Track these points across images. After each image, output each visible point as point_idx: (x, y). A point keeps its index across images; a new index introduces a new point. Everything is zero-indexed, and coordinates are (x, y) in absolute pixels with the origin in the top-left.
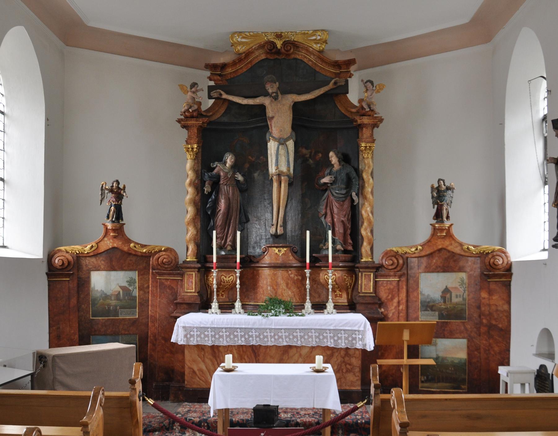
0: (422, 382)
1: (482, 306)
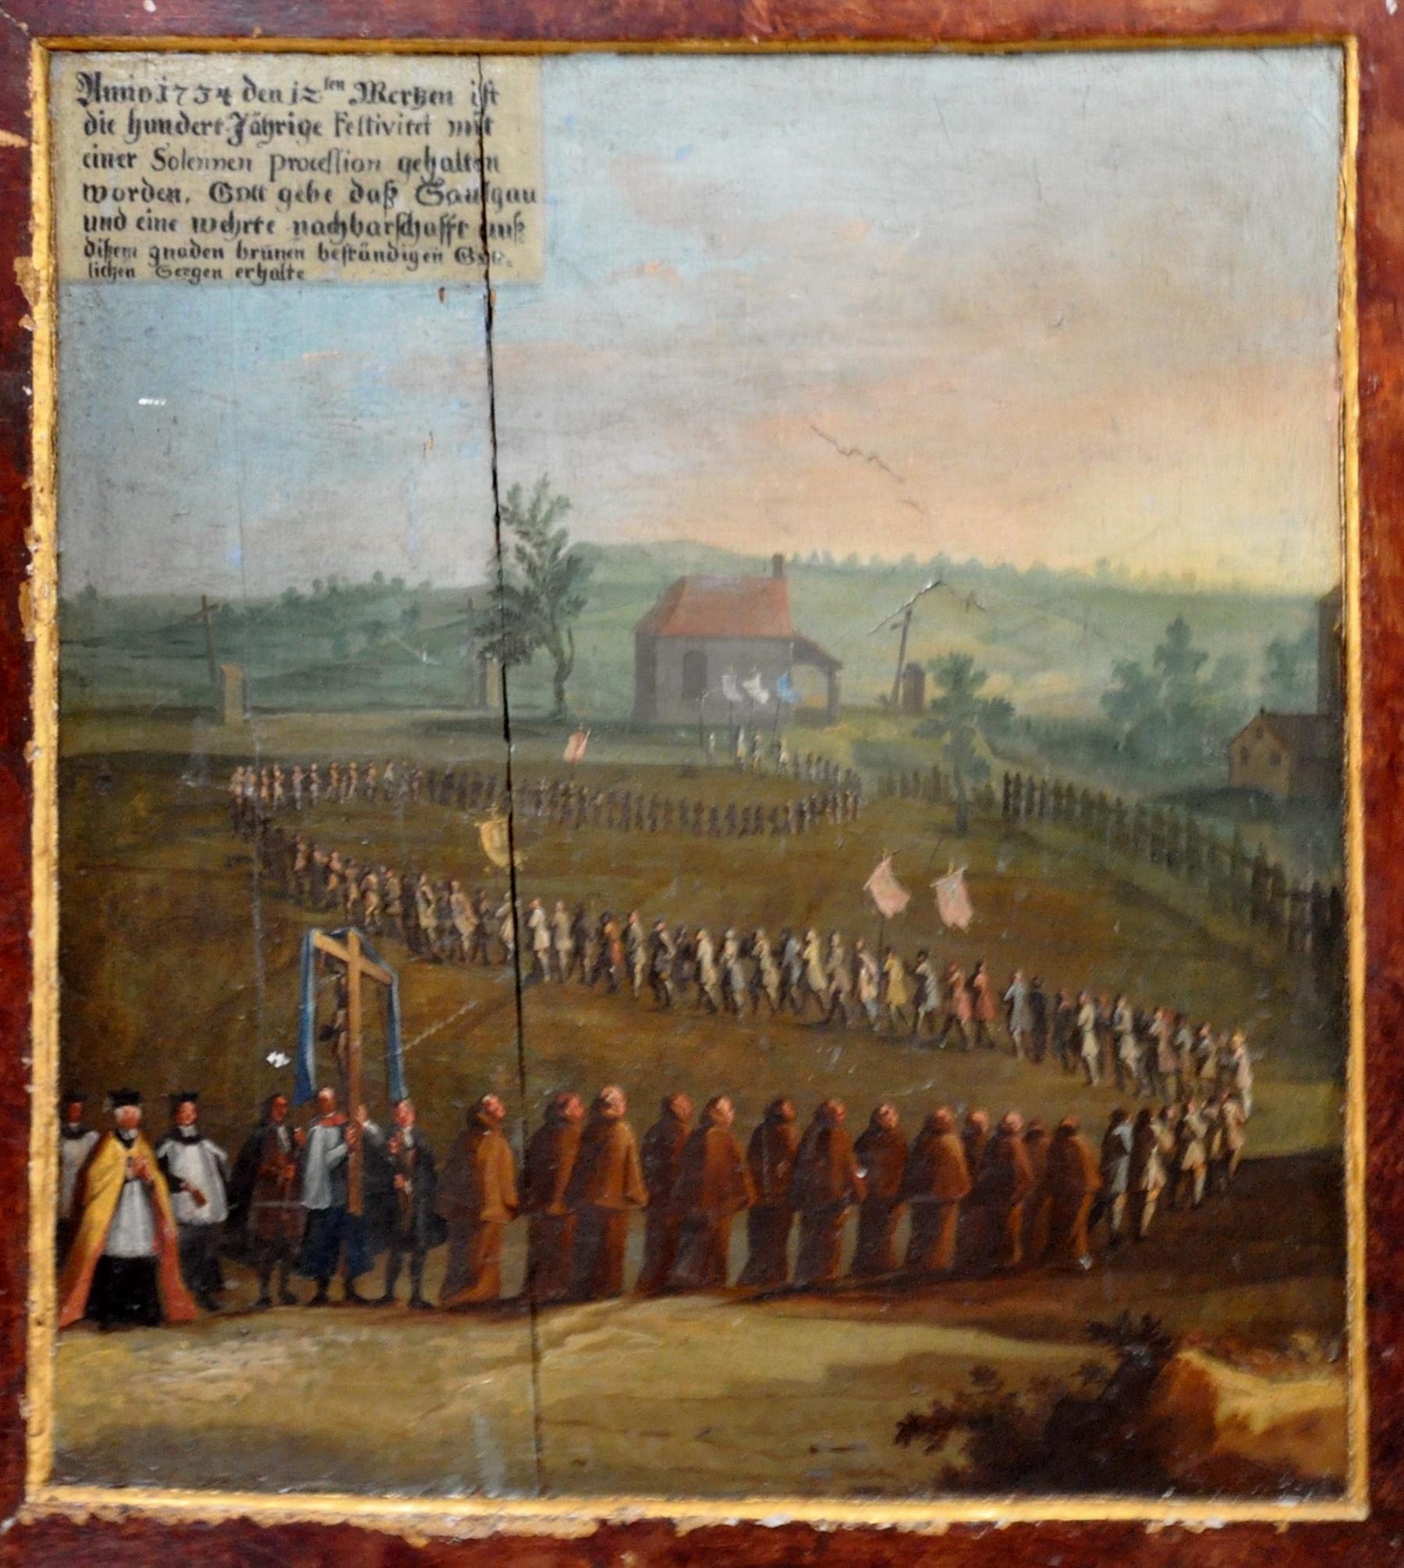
0: (119, 1297)
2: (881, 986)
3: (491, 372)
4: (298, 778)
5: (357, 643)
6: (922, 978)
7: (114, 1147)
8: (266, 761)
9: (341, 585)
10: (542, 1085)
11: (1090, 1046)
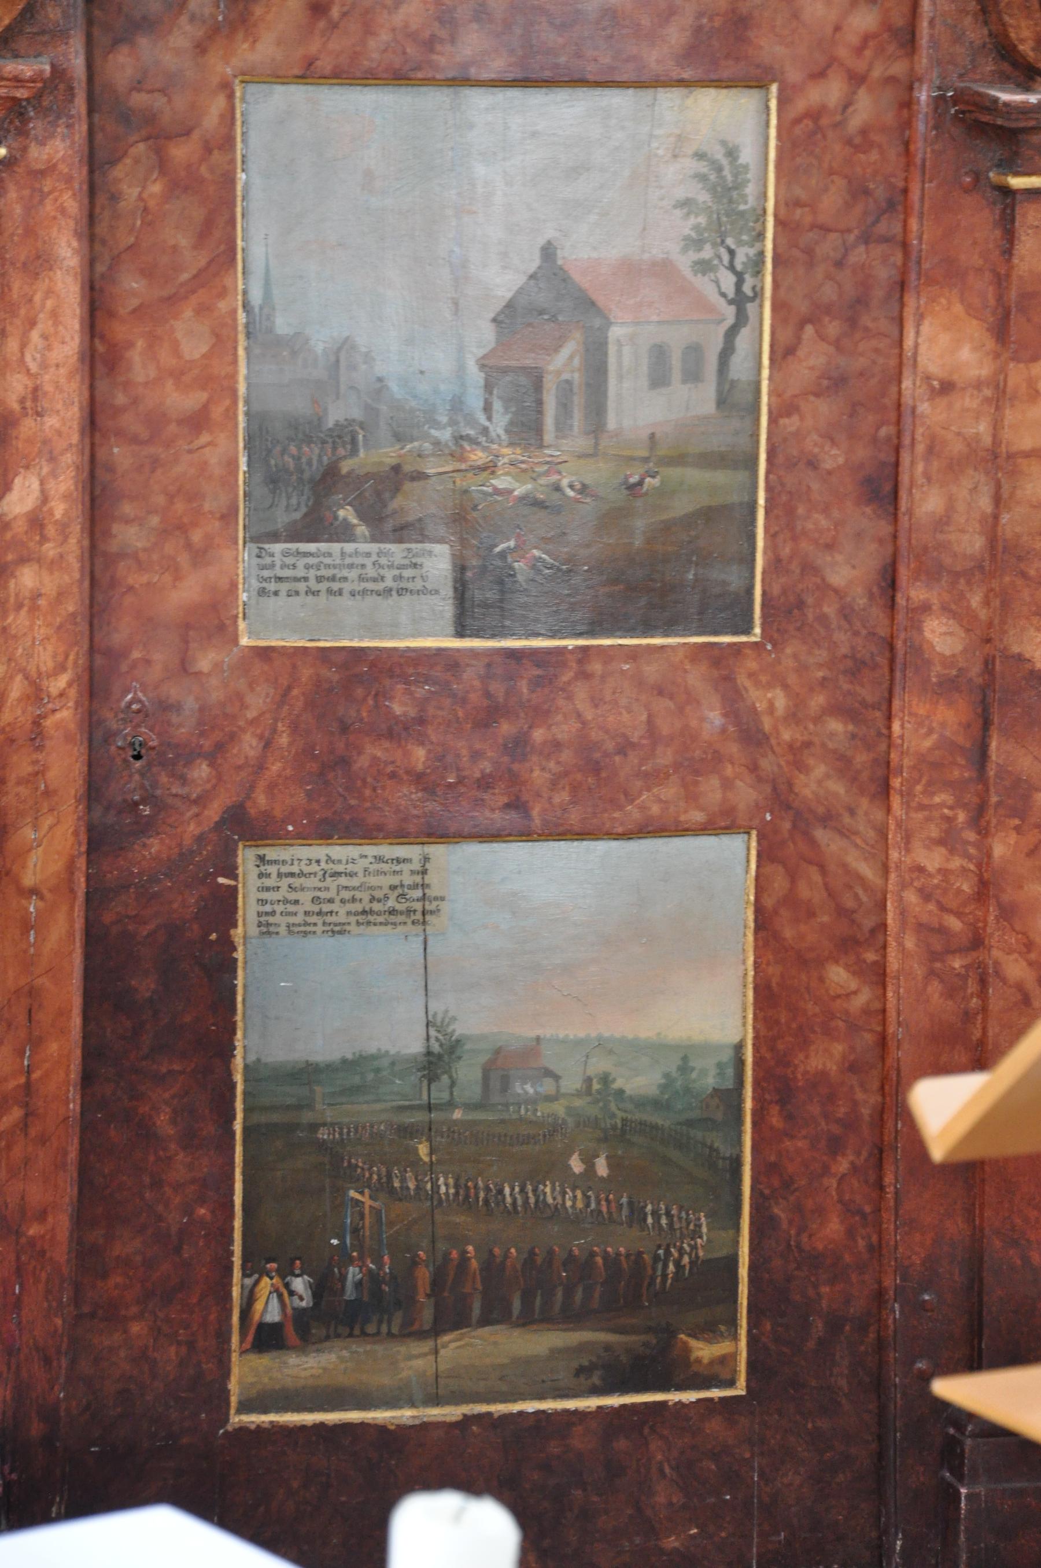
0: (267, 1339)
1: (914, 468)
2: (573, 1201)
3: (426, 968)
4: (345, 1130)
5: (370, 1076)
6: (589, 1197)
7: (266, 1280)
8: (333, 1125)
9: (364, 1053)
10: (441, 1246)
11: (650, 1220)
